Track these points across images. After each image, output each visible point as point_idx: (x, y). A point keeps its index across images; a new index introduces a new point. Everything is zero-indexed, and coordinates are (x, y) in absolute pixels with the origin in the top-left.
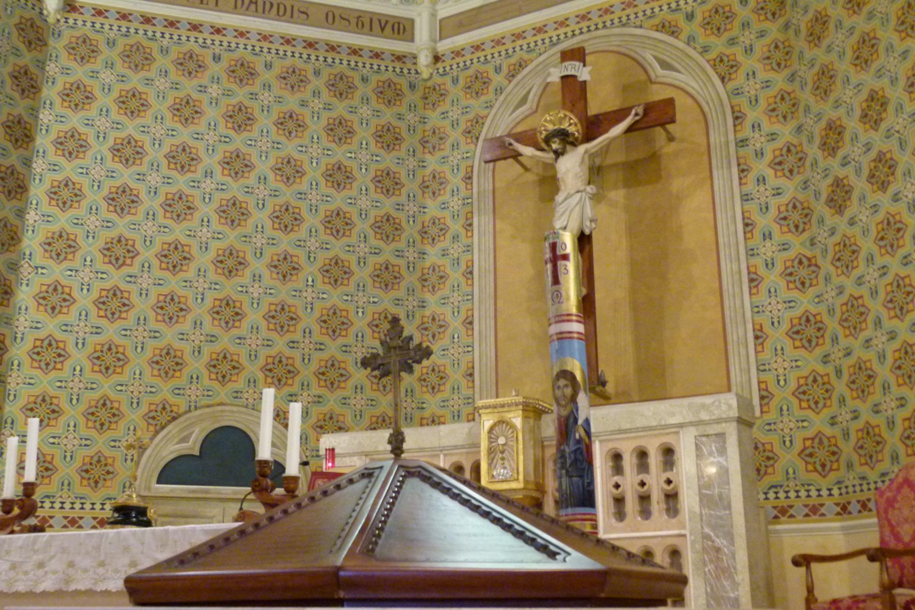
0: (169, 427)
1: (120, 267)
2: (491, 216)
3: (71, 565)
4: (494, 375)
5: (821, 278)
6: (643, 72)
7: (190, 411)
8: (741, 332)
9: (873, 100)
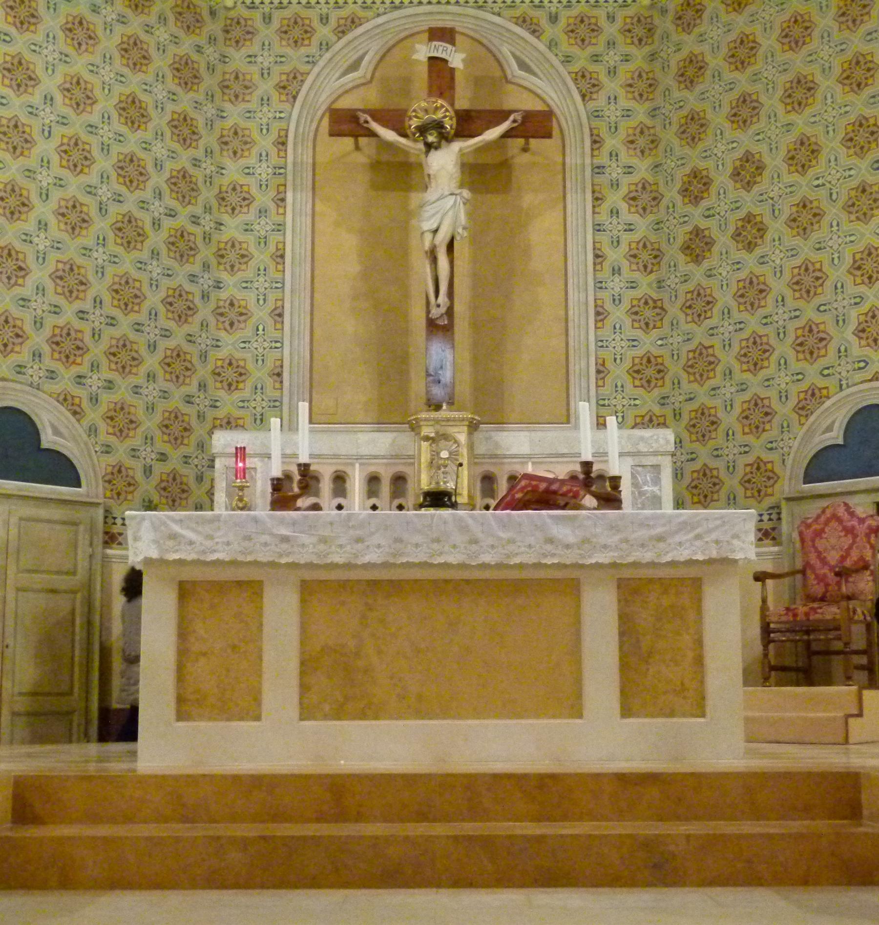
2: (310, 194)
8: (583, 364)
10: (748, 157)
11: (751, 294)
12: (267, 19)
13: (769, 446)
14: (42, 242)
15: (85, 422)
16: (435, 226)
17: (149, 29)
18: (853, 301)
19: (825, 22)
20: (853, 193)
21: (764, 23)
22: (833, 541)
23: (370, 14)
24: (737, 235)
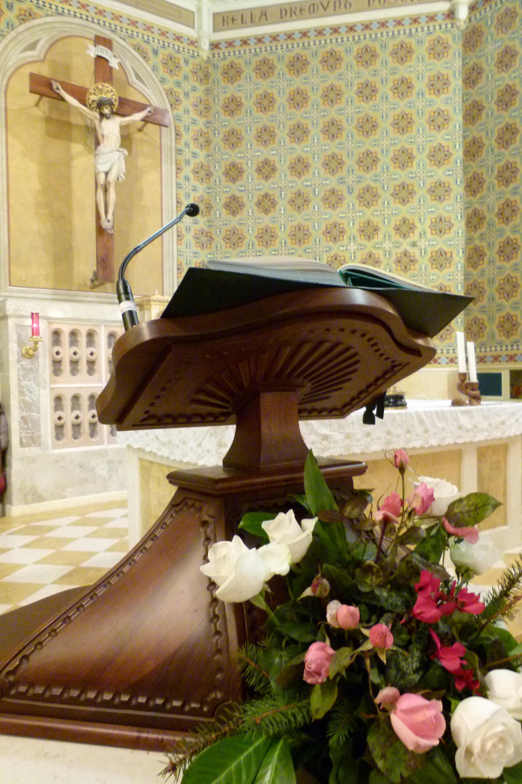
2: (4, 130)
3: (389, 433)
4: (7, 254)
5: (213, 245)
6: (124, 75)
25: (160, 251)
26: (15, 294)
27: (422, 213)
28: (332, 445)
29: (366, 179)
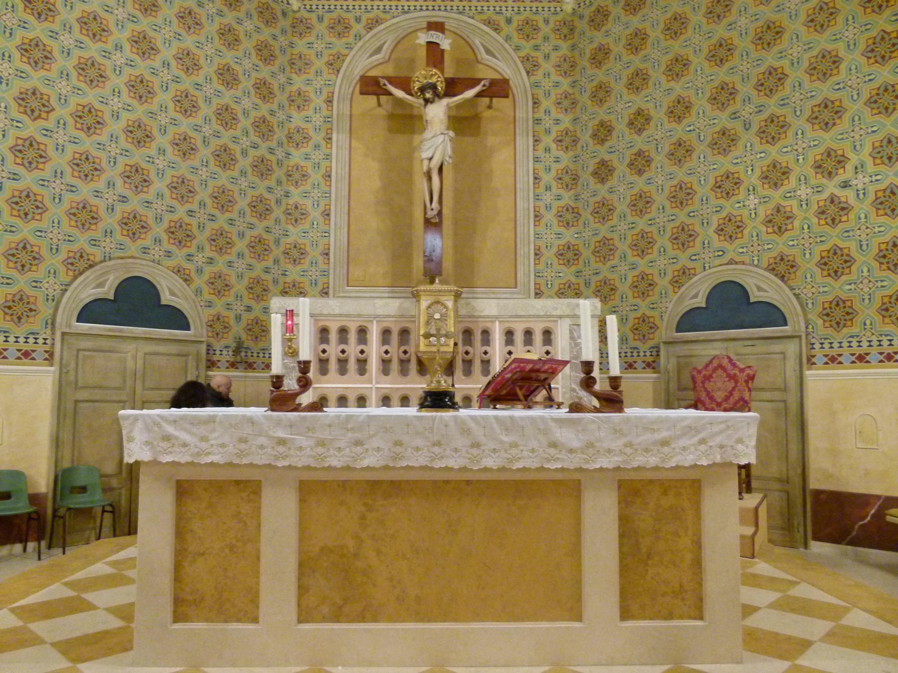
0: (87, 273)
1: (35, 119)
2: (348, 135)
5: (581, 222)
7: (105, 261)
8: (526, 250)
9: (639, 114)
10: (639, 113)
11: (641, 205)
12: (320, 19)
13: (652, 306)
14: (161, 163)
15: (194, 286)
16: (430, 155)
17: (239, 22)
18: (714, 210)
19: (697, 18)
20: (716, 136)
21: (652, 20)
22: (719, 384)
23: (388, 16)
24: (631, 165)
25: (513, 236)
26: (352, 295)
27: (857, 137)
28: (292, 452)
29: (770, 106)
